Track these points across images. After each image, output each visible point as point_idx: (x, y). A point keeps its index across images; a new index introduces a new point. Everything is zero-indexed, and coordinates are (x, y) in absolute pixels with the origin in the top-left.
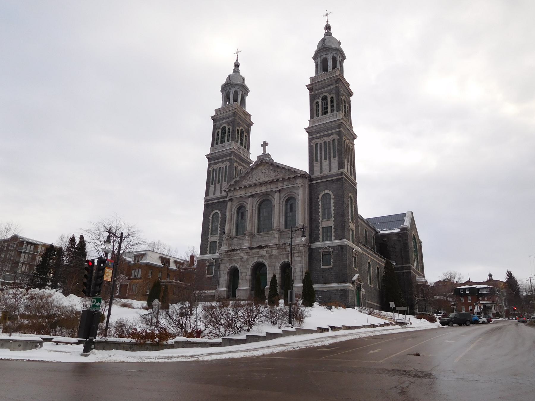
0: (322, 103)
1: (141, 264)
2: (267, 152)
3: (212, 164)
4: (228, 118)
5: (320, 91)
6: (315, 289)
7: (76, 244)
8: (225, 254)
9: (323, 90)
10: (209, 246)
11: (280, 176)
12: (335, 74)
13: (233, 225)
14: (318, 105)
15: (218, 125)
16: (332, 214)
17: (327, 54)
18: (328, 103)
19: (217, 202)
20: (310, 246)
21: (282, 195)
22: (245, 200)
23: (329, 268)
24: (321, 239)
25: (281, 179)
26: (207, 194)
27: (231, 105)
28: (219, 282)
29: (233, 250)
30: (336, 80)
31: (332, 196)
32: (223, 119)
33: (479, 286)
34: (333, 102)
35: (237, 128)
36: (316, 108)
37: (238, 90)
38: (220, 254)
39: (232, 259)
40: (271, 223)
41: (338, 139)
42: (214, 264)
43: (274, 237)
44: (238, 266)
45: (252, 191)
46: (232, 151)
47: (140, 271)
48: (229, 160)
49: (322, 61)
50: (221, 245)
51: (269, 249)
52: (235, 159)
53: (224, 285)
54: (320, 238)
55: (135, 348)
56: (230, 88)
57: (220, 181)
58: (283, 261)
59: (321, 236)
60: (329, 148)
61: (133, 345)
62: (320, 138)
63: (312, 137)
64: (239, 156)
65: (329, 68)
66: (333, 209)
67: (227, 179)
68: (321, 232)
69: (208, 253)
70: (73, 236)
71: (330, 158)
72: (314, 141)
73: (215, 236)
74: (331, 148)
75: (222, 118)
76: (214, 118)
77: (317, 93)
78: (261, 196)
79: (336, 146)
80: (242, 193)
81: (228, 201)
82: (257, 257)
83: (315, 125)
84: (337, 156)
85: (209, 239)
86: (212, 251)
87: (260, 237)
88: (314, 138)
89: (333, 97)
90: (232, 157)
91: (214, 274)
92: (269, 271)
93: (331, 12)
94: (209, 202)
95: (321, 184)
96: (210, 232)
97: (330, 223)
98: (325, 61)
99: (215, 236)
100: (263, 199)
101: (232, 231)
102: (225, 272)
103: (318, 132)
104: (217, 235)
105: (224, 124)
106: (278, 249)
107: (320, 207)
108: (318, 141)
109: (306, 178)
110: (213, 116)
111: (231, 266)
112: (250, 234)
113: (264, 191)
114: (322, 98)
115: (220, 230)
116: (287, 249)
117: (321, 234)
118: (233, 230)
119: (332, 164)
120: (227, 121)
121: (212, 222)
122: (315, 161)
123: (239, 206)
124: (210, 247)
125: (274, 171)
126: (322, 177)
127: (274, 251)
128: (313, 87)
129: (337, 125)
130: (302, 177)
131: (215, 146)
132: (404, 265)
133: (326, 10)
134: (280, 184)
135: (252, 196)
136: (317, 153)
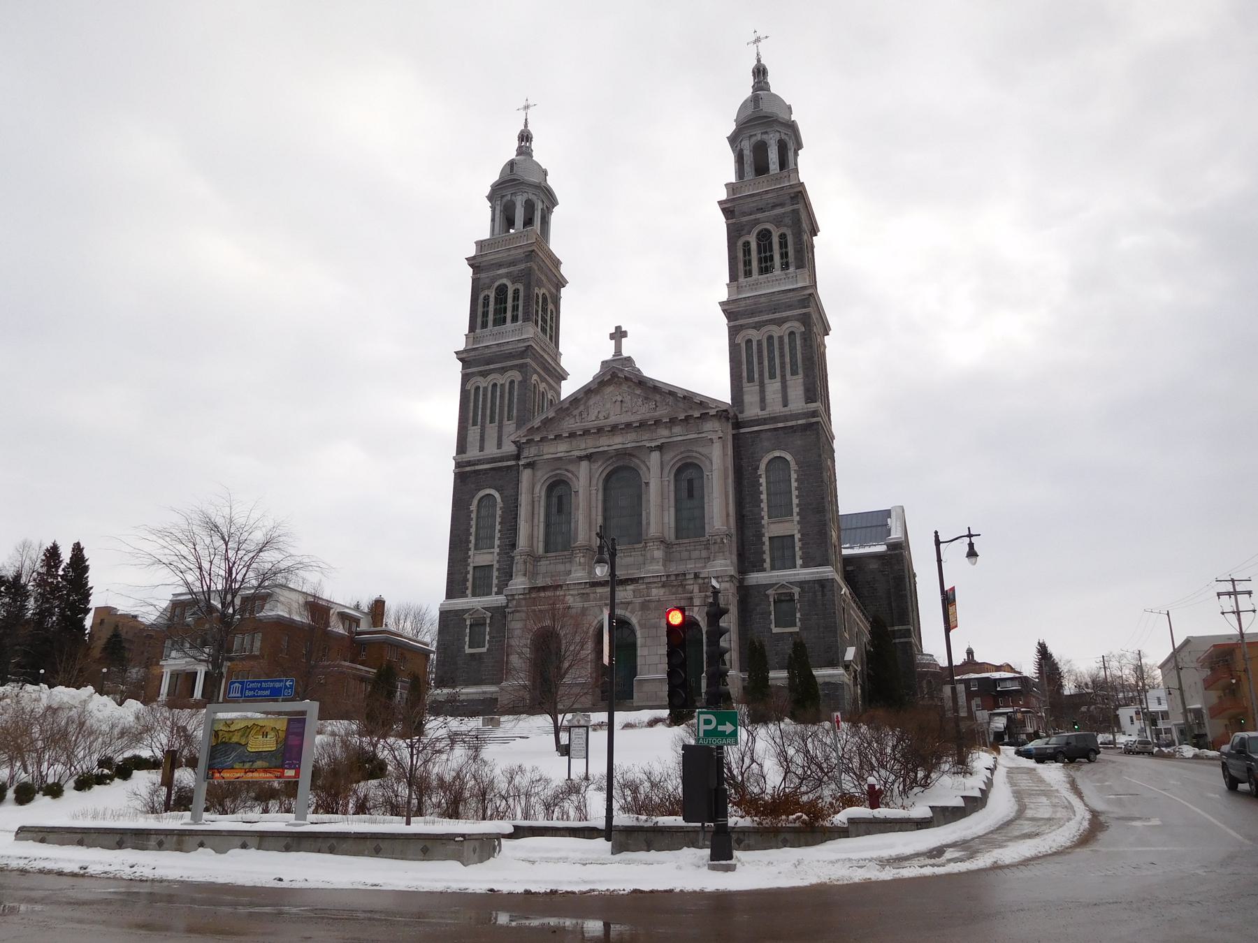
0: (759, 246)
1: (260, 620)
2: (625, 353)
3: (473, 374)
4: (513, 263)
5: (753, 217)
7: (62, 566)
8: (521, 597)
9: (759, 216)
10: (470, 576)
11: (663, 412)
12: (789, 181)
13: (538, 526)
14: (750, 248)
15: (487, 281)
16: (794, 506)
17: (766, 133)
20: (741, 581)
21: (667, 457)
22: (570, 467)
23: (791, 632)
24: (767, 565)
25: (668, 420)
27: (520, 235)
30: (792, 195)
32: (500, 265)
33: (997, 675)
34: (786, 247)
35: (536, 289)
36: (745, 256)
37: (534, 198)
38: (509, 598)
40: (641, 523)
41: (804, 332)
42: (488, 621)
43: (653, 558)
47: (259, 637)
48: (522, 368)
49: (753, 148)
50: (507, 575)
51: (641, 587)
52: (536, 367)
55: (752, 842)
57: (497, 417)
59: (767, 557)
60: (780, 353)
61: (744, 835)
62: (757, 326)
63: (737, 323)
64: (541, 360)
67: (515, 414)
68: (766, 547)
69: (470, 595)
70: (54, 544)
71: (783, 377)
72: (743, 333)
74: (786, 352)
76: (473, 263)
78: (611, 458)
79: (799, 347)
80: (561, 449)
81: (524, 468)
83: (744, 296)
84: (800, 371)
86: (481, 589)
88: (741, 326)
89: (785, 235)
90: (528, 360)
93: (767, 37)
94: (468, 469)
95: (763, 435)
96: (473, 541)
97: (791, 527)
98: (760, 150)
101: (535, 539)
103: (752, 314)
104: (492, 550)
105: (502, 278)
106: (663, 586)
107: (763, 488)
108: (754, 334)
109: (728, 419)
110: (474, 258)
113: (620, 446)
114: (758, 234)
115: (499, 539)
117: (768, 552)
118: (538, 538)
119: (789, 390)
120: (510, 272)
121: (478, 518)
122: (745, 380)
123: (551, 481)
124: (474, 578)
125: (646, 398)
126: (765, 419)
127: (654, 591)
129: (799, 301)
130: (721, 416)
131: (478, 331)
132: (896, 628)
133: (755, 31)
134: (664, 432)
135: (589, 457)
136: (750, 363)
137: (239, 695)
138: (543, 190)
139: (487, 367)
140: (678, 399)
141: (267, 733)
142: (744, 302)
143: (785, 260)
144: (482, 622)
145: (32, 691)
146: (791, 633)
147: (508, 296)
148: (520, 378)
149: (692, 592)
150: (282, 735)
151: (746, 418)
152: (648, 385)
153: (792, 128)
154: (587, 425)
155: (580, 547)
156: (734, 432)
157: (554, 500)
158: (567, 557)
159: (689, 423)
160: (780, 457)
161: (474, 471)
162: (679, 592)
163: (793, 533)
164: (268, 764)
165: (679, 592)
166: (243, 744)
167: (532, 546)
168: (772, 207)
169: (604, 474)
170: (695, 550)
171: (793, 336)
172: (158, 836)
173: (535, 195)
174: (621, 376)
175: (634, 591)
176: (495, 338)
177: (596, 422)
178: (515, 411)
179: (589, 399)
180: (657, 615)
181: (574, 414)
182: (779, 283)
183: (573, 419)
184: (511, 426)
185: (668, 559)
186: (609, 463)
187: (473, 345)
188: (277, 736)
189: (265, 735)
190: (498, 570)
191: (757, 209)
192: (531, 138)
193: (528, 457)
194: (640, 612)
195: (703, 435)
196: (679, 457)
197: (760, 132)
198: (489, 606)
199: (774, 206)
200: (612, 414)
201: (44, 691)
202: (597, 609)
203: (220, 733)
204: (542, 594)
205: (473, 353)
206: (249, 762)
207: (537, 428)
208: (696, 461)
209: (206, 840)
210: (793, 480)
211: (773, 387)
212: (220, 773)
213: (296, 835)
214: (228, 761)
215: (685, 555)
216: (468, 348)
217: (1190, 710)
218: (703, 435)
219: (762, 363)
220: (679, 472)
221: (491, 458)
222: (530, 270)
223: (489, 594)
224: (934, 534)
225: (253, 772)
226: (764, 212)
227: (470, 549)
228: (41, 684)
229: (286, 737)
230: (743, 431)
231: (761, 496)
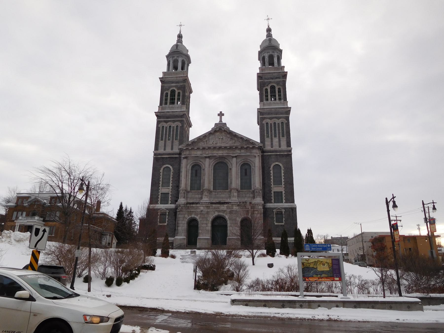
0: (271, 91)
2: (224, 121)
5: (269, 80)
6: (288, 241)
8: (183, 206)
9: (271, 80)
10: (160, 197)
11: (237, 144)
14: (268, 91)
16: (283, 182)
17: (274, 52)
18: (176, 96)
22: (201, 160)
24: (273, 201)
26: (157, 147)
27: (181, 72)
29: (190, 203)
30: (283, 75)
31: (282, 168)
32: (172, 82)
36: (266, 93)
39: (190, 211)
41: (287, 123)
42: (167, 214)
44: (197, 218)
45: (209, 153)
48: (182, 121)
53: (183, 234)
54: (272, 200)
56: (179, 56)
59: (273, 198)
62: (271, 118)
65: (179, 69)
67: (178, 138)
68: (273, 195)
69: (159, 204)
71: (279, 137)
73: (166, 188)
77: (267, 82)
78: (217, 158)
80: (199, 153)
84: (285, 136)
85: (160, 191)
86: (165, 200)
87: (216, 193)
88: (265, 117)
89: (180, 92)
91: (167, 223)
93: (184, 25)
96: (161, 184)
98: (176, 62)
99: (166, 188)
100: (218, 161)
102: (183, 222)
103: (269, 114)
104: (169, 187)
106: (238, 206)
107: (272, 174)
108: (165, 125)
111: (190, 217)
112: (209, 190)
113: (221, 155)
114: (171, 91)
116: (247, 207)
119: (281, 142)
122: (266, 137)
125: (231, 139)
126: (273, 151)
127: (234, 207)
128: (263, 76)
133: (268, 16)
137: (309, 249)
138: (171, 54)
139: (168, 120)
140: (244, 140)
141: (324, 264)
143: (280, 97)
144: (164, 214)
145: (7, 233)
146: (281, 225)
147: (176, 94)
148: (181, 125)
149: (248, 209)
150: (331, 265)
151: (266, 150)
153: (281, 51)
154: (210, 146)
155: (206, 189)
156: (262, 154)
157: (194, 172)
158: (199, 192)
164: (327, 276)
166: (315, 268)
167: (186, 188)
169: (214, 164)
170: (248, 194)
172: (299, 303)
173: (185, 58)
174: (223, 129)
175: (227, 207)
176: (169, 109)
177: (212, 145)
178: (178, 137)
180: (235, 216)
181: (204, 141)
182: (278, 105)
183: (204, 143)
184: (176, 142)
185: (238, 196)
187: (162, 110)
188: (328, 265)
189: (324, 265)
190: (171, 195)
191: (271, 78)
192: (271, 30)
193: (185, 155)
196: (242, 161)
197: (271, 51)
198: (168, 208)
199: (277, 78)
200: (218, 142)
201: (11, 233)
203: (305, 264)
204: (192, 205)
205: (162, 114)
206: (319, 274)
209: (321, 304)
210: (282, 173)
211: (276, 140)
212: (308, 278)
213: (357, 302)
214: (310, 274)
216: (159, 111)
217: (343, 253)
220: (242, 166)
221: (169, 153)
222: (185, 86)
223: (168, 203)
224: (422, 202)
225: (321, 278)
226: (273, 79)
227: (160, 186)
228: (10, 230)
229: (332, 266)
230: (265, 154)
231: (271, 177)
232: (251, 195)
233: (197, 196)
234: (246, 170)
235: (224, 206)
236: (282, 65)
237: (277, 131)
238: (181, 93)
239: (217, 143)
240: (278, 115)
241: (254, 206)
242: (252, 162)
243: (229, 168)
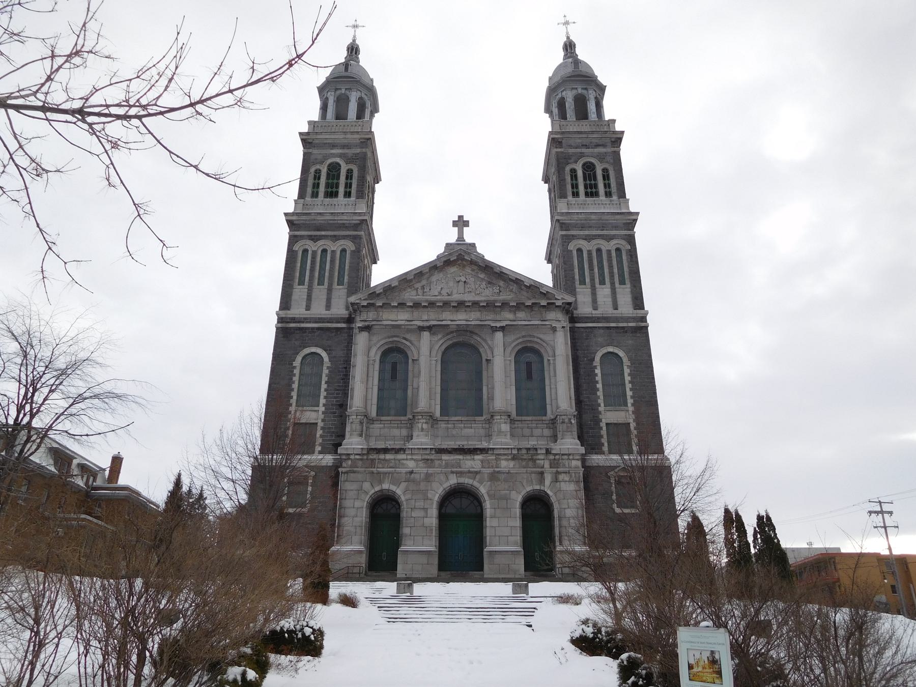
0: (584, 174)
5: (579, 150)
8: (357, 457)
9: (584, 150)
14: (352, 175)
15: (320, 157)
19: (319, 329)
26: (286, 302)
28: (341, 528)
29: (378, 451)
30: (613, 140)
34: (609, 179)
36: (572, 179)
39: (379, 473)
42: (310, 481)
44: (399, 491)
46: (364, 220)
51: (490, 458)
53: (356, 539)
54: (603, 445)
58: (529, 489)
62: (588, 238)
66: (631, 387)
68: (604, 432)
75: (331, 143)
78: (452, 332)
80: (402, 317)
82: (457, 473)
84: (627, 281)
87: (450, 426)
88: (573, 236)
89: (320, 170)
92: (493, 510)
93: (347, 26)
98: (562, 105)
100: (455, 341)
102: (358, 504)
103: (583, 227)
104: (316, 408)
107: (599, 378)
108: (311, 246)
111: (377, 489)
113: (464, 323)
120: (344, 154)
122: (577, 282)
125: (490, 283)
126: (598, 318)
127: (504, 463)
129: (624, 224)
142: (577, 216)
147: (341, 174)
148: (353, 248)
149: (543, 467)
152: (495, 270)
153: (371, 91)
155: (423, 413)
156: (571, 325)
159: (533, 311)
160: (617, 354)
161: (299, 328)
162: (530, 466)
163: (628, 422)
165: (530, 466)
167: (366, 408)
168: (595, 146)
169: (443, 348)
170: (537, 428)
171: (344, 253)
175: (482, 461)
176: (321, 206)
177: (439, 297)
179: (431, 275)
180: (506, 487)
186: (449, 337)
190: (322, 428)
193: (366, 321)
194: (489, 483)
195: (547, 323)
196: (521, 340)
199: (597, 146)
200: (455, 291)
202: (443, 477)
204: (382, 456)
205: (304, 218)
207: (378, 294)
208: (536, 346)
211: (604, 292)
215: (527, 432)
218: (547, 323)
219: (593, 270)
226: (588, 148)
232: (547, 432)
233: (396, 432)
234: (529, 365)
235: (474, 459)
236: (607, 117)
237: (606, 271)
238: (354, 171)
239: (452, 292)
240: (606, 230)
241: (559, 459)
242: (544, 344)
243: (484, 358)
